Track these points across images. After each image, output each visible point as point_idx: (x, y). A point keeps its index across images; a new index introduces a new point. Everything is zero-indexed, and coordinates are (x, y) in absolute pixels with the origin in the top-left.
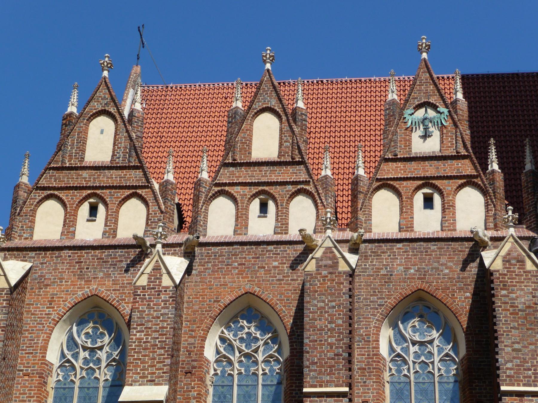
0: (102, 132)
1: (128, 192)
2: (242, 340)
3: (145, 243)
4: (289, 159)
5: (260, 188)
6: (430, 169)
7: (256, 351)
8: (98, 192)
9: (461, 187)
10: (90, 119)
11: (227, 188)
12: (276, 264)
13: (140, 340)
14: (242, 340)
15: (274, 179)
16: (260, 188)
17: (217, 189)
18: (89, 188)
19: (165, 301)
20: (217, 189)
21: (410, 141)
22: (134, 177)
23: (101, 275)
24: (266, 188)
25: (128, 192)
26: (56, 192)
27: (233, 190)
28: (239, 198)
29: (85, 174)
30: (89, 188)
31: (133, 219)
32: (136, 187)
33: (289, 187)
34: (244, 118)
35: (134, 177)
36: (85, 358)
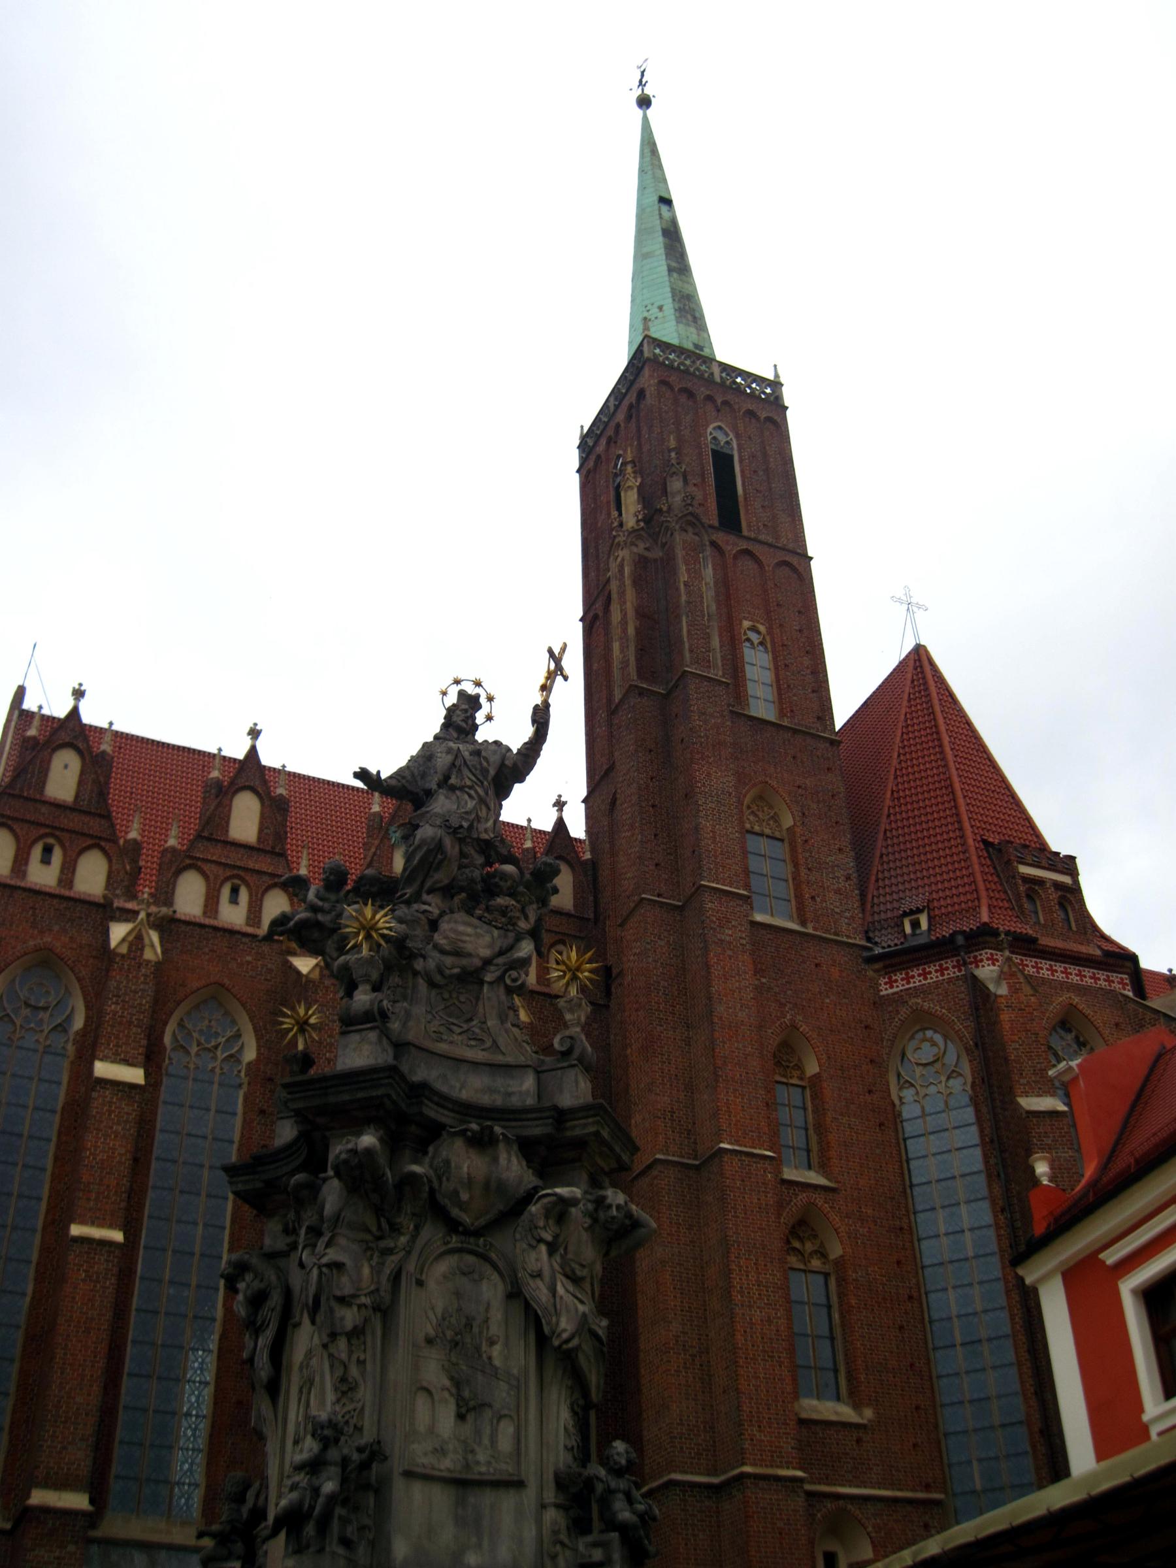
0: (66, 767)
1: (90, 842)
2: (201, 1032)
3: (112, 904)
4: (269, 848)
5: (235, 872)
6: (234, 858)
7: (216, 1047)
8: (58, 833)
9: (275, 885)
10: (54, 750)
11: (199, 863)
12: (249, 958)
13: (115, 1013)
14: (201, 1032)
15: (251, 865)
16: (235, 872)
17: (188, 861)
18: (48, 826)
19: (146, 976)
20: (188, 861)
21: (392, 859)
22: (95, 826)
23: (56, 928)
24: (242, 873)
25: (90, 842)
26: (10, 822)
27: (207, 867)
28: (212, 877)
29: (44, 809)
30: (48, 826)
31: (92, 875)
32: (100, 838)
33: (265, 878)
34: (226, 793)
35: (95, 826)
36: (27, 1017)
